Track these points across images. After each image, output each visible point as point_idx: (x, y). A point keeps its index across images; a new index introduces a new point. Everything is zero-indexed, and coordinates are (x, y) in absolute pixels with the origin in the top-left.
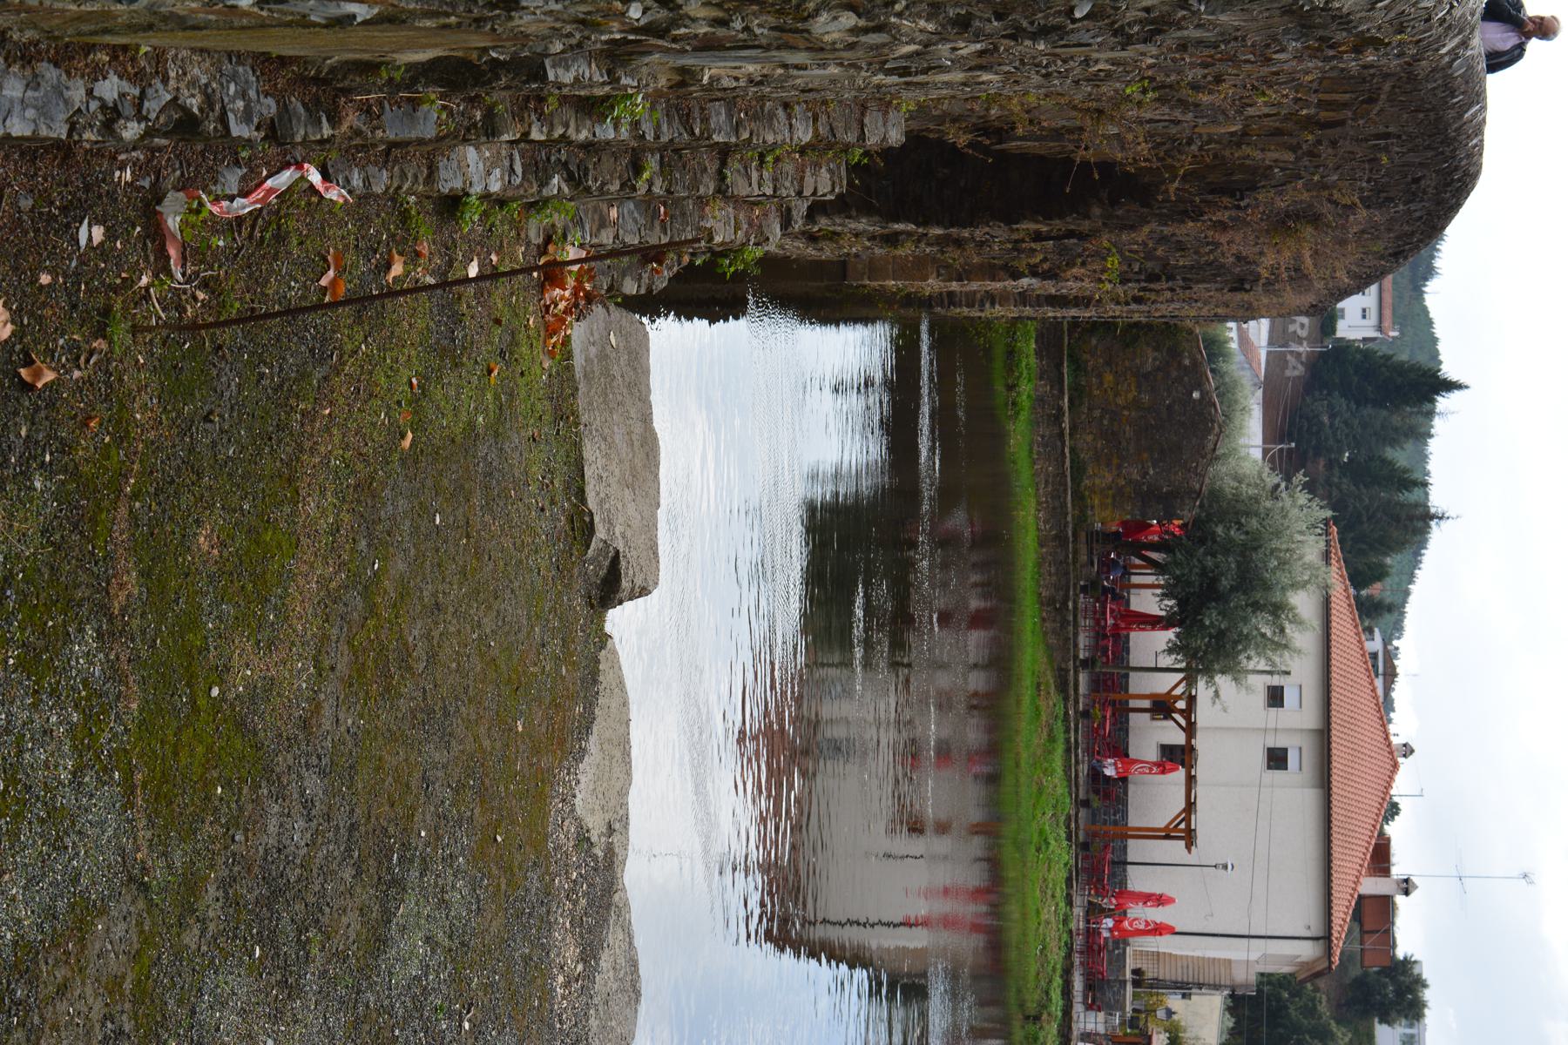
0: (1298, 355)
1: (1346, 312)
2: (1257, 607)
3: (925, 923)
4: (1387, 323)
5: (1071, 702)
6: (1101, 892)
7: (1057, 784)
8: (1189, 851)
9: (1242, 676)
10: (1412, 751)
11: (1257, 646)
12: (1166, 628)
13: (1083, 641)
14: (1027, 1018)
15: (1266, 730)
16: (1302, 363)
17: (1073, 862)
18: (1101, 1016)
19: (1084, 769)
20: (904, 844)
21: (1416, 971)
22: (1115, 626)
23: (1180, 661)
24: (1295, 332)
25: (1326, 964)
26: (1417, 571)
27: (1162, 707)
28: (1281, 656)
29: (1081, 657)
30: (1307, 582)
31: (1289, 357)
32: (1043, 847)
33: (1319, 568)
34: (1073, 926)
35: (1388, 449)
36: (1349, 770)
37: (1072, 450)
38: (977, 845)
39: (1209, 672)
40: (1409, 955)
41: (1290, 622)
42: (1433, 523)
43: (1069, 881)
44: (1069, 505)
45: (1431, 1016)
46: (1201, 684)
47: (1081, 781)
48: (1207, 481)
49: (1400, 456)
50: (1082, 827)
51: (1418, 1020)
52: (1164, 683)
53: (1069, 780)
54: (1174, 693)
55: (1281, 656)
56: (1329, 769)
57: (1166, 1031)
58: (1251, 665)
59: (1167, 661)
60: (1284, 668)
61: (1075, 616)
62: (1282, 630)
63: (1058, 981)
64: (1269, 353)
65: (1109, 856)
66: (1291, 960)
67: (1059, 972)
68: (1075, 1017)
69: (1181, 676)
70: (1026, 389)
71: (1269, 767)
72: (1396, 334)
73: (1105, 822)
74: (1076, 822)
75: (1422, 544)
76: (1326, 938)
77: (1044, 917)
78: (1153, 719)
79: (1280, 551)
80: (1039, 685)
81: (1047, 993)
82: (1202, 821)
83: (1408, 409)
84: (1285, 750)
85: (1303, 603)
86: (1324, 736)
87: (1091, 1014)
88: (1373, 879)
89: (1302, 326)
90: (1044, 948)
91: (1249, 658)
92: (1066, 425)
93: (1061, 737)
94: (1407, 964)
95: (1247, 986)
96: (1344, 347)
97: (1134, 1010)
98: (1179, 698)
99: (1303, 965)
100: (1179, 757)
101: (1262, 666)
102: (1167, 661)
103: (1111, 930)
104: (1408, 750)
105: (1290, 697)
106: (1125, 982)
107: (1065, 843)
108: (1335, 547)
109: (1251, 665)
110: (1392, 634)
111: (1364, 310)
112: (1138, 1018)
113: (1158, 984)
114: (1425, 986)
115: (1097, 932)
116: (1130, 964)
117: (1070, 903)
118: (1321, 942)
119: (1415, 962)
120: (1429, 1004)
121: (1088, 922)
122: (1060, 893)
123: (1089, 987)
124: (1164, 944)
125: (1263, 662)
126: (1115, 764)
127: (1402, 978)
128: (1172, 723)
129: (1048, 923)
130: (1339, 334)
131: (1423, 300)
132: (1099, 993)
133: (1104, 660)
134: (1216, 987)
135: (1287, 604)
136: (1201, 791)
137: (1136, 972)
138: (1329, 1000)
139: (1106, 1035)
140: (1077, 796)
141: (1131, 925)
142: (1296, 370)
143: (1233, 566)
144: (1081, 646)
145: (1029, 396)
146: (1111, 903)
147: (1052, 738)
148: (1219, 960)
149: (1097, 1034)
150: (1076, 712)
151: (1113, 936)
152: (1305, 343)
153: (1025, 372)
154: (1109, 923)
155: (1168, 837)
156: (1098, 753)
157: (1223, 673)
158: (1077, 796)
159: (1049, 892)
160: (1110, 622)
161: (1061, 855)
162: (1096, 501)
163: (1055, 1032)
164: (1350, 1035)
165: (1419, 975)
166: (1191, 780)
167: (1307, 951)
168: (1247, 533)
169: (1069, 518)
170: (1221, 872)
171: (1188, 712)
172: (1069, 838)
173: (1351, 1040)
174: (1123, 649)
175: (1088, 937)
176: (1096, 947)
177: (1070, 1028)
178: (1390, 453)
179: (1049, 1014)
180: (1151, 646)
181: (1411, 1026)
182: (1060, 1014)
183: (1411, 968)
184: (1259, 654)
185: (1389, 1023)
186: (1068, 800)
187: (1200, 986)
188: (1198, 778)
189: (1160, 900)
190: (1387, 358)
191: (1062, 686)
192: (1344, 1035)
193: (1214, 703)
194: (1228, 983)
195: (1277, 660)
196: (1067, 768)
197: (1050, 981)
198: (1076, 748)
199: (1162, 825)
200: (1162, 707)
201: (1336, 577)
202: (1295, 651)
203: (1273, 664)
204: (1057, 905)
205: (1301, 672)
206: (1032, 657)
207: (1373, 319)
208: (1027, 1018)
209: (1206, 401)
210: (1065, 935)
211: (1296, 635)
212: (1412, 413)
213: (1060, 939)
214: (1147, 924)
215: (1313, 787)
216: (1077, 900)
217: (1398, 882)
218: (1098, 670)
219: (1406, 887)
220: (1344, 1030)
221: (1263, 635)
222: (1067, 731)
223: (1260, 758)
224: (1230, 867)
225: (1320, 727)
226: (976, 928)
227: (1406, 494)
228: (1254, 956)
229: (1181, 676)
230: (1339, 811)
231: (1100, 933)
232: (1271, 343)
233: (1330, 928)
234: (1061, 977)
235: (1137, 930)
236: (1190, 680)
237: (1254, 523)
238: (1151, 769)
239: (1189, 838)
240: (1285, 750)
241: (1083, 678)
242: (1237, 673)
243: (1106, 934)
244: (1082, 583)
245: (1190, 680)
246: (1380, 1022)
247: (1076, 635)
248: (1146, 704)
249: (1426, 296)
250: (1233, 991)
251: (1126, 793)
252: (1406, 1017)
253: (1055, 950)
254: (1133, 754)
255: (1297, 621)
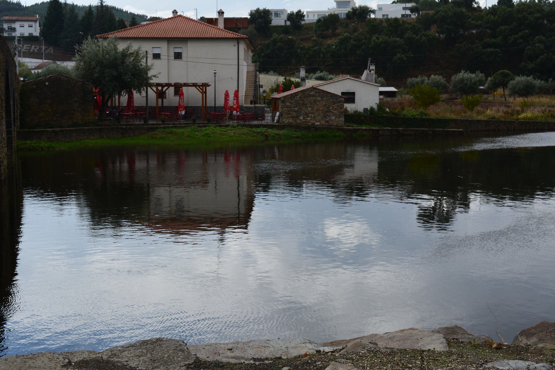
0: (45, 49)
1: (30, 32)
2: (123, 62)
3: (238, 177)
4: (34, 19)
5: (159, 126)
6: (225, 115)
7: (186, 131)
8: (210, 85)
9: (148, 67)
10: (175, 10)
11: (137, 62)
12: (132, 94)
13: (137, 122)
14: (267, 139)
15: (168, 60)
16: (49, 48)
17: (214, 125)
18: (266, 115)
19: (182, 121)
20: (211, 185)
21: (254, 12)
22: (132, 111)
23: (144, 89)
24: (37, 50)
25: (246, 39)
26: (116, 8)
27: (161, 95)
28: (141, 54)
29: (143, 123)
30: (114, 45)
31: (46, 52)
32: (209, 135)
33: (109, 41)
34: (236, 125)
35: (79, 18)
36: (181, 31)
37: (68, 127)
38: (211, 160)
39: (148, 79)
40: (249, 14)
41: (128, 51)
42: (104, 4)
43: (220, 126)
44: (88, 128)
45: (269, 7)
46: (151, 81)
47: (187, 122)
48: (79, 80)
49: (81, 15)
50: (202, 122)
51: (270, 11)
52: (152, 93)
53: (186, 126)
54: (155, 90)
55: (141, 54)
56: (181, 38)
57: (273, 93)
58: (144, 64)
59: (144, 93)
60: (145, 53)
61: (128, 125)
62: (132, 53)
63: (254, 129)
64: (45, 59)
65: (213, 112)
66: (246, 52)
67: (251, 129)
68: (266, 123)
69: (149, 88)
70: (44, 144)
71: (181, 58)
72: (37, 16)
73: (201, 114)
74: (200, 124)
75: (114, 8)
76: (238, 40)
77: (232, 134)
78: (166, 98)
79: (103, 54)
80: (153, 138)
81: (258, 133)
82: (200, 80)
83: (64, 11)
84: (175, 53)
85: (121, 46)
86: (170, 40)
87: (266, 118)
88: (219, 24)
89: (35, 48)
90: (243, 134)
91: (141, 65)
92: (58, 129)
93: (171, 129)
94: (251, 14)
95: (255, 66)
96: (42, 33)
97: (264, 103)
98: (157, 89)
99: (248, 47)
100: (178, 88)
101: (144, 60)
102: (144, 93)
103: (237, 112)
104: (175, 12)
105: (157, 51)
106: (255, 107)
107: (207, 128)
108: (104, 35)
109: (144, 64)
110: (145, 19)
111: (29, 26)
112: (267, 102)
113: (255, 96)
114: (259, 9)
115: (238, 116)
116: (249, 105)
117: (228, 126)
118: (239, 41)
119: (251, 12)
120: (264, 8)
121: (235, 119)
122: (224, 129)
123: (257, 119)
124: (242, 94)
125: (143, 60)
126: (180, 111)
127: (256, 16)
128: (167, 91)
129: (234, 133)
130: (38, 35)
131: (29, 6)
132: (259, 115)
133: (144, 115)
134: (256, 76)
135: (122, 51)
136: (191, 81)
137: (251, 103)
138: (264, 40)
139: (272, 113)
140: (191, 124)
141: (235, 105)
142: (51, 50)
143: (108, 70)
144: (139, 123)
145: (46, 143)
146: (228, 112)
147: (171, 133)
148: (247, 75)
149: (272, 116)
150: (162, 124)
151: (239, 111)
152: (42, 47)
153: (37, 144)
154: (235, 112)
155: (205, 93)
156: (177, 116)
157: (147, 74)
158: (191, 124)
159: (224, 133)
160: (131, 113)
161: (211, 129)
162: (87, 118)
163: (271, 130)
164: (275, 33)
165: (255, 11)
166: (186, 85)
167: (242, 46)
168: (97, 66)
169: (93, 128)
170: (217, 75)
171: (162, 85)
172: (205, 126)
173: (277, 33)
174: (141, 109)
175: (240, 119)
176: (243, 117)
177: (270, 125)
178: (80, 18)
179: (265, 132)
180: (139, 98)
181: (272, 14)
182: (265, 129)
183: (253, 13)
184: (140, 62)
185: (271, 20)
186: (193, 127)
187: (256, 82)
188: (185, 82)
189: (227, 95)
190: (46, 18)
191: (153, 129)
192: (275, 36)
193: (157, 77)
194: (255, 72)
195: (142, 55)
196: (181, 127)
197: (254, 132)
198: (175, 124)
199: (201, 95)
200: (161, 95)
201: (111, 36)
202: (139, 49)
203: (143, 57)
204: (228, 130)
205: (147, 47)
206: (142, 140)
207: (33, 23)
208: (267, 139)
209: (49, 80)
210: (239, 127)
211: (133, 49)
212: (65, 10)
213: (240, 129)
214: (234, 99)
215: (187, 43)
216: (227, 123)
217: (219, 15)
218: (148, 117)
219: (221, 13)
220: (273, 36)
221: (133, 60)
222: (168, 127)
223: (178, 62)
224: (215, 72)
225: (167, 41)
226: (238, 159)
227: (94, 12)
228: (245, 64)
229: (149, 88)
230: (195, 35)
231: (238, 115)
232: (41, 58)
233: (234, 38)
234: (253, 128)
235: (237, 103)
236: (151, 85)
237: (93, 63)
238: (182, 98)
239: (206, 85)
240: (175, 53)
241: (150, 122)
242: (147, 69)
243: (238, 113)
244: (117, 123)
245: (151, 85)
246: (271, 24)
247: (135, 125)
248: (160, 100)
249: (27, 6)
250: (257, 71)
251: (192, 107)
252: (269, 15)
253: (244, 130)
254: (177, 105)
255: (128, 48)
